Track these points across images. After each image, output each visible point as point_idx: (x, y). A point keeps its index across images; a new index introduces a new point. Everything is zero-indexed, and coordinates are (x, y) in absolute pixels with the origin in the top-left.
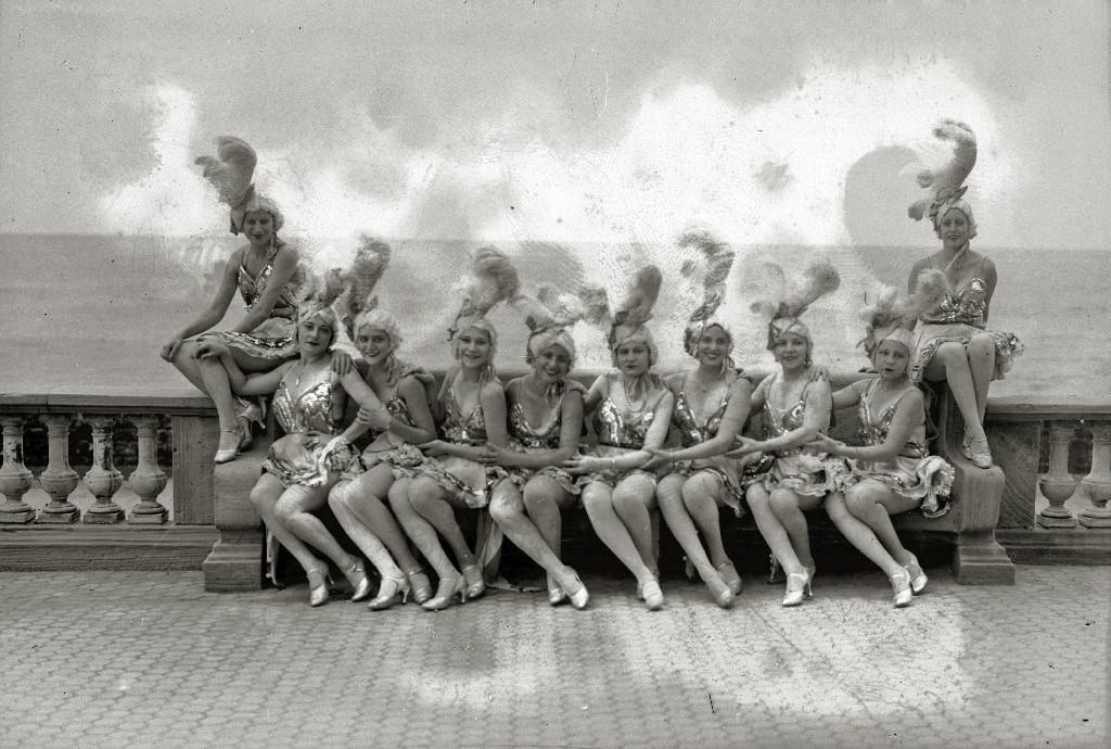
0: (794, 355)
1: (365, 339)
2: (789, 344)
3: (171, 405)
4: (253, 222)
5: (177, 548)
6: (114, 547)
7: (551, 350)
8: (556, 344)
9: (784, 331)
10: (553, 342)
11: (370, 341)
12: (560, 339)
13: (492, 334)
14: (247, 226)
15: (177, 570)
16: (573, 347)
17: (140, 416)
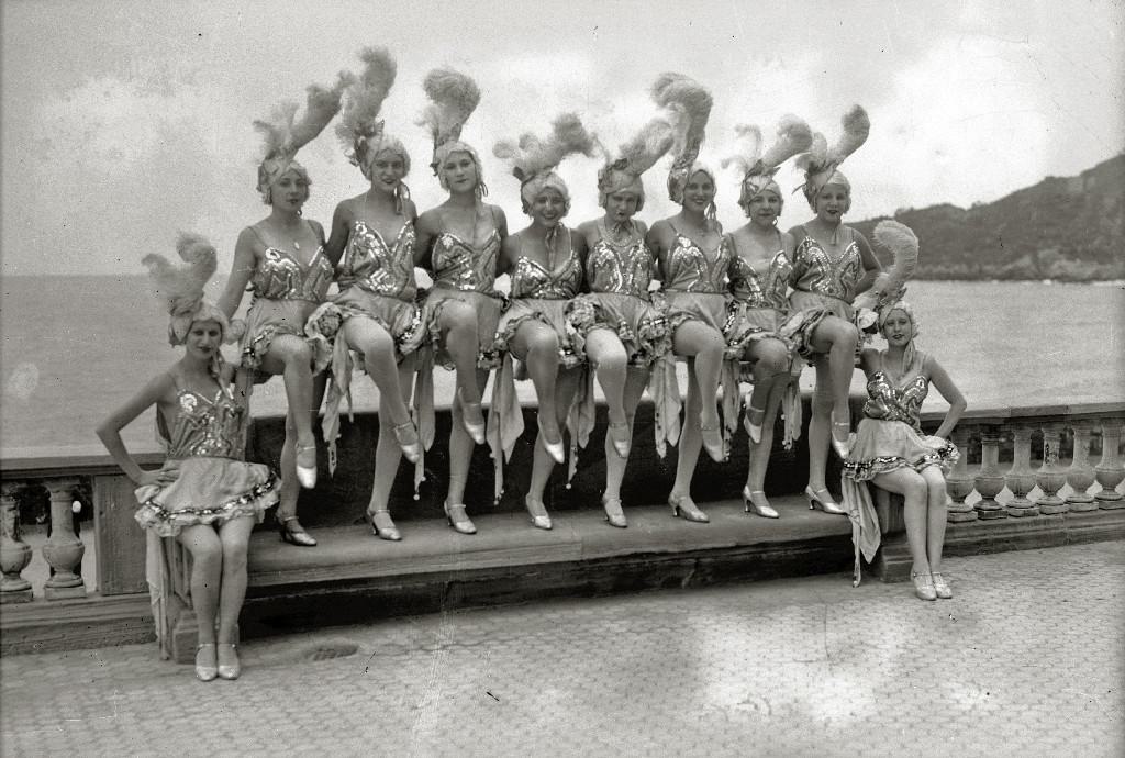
0: (770, 212)
1: (383, 164)
2: (766, 201)
3: (99, 464)
4: (200, 333)
5: (110, 622)
6: (36, 627)
7: (545, 194)
8: (548, 187)
9: (761, 188)
10: (544, 185)
11: (390, 167)
12: (550, 183)
13: (473, 152)
14: (193, 338)
15: (111, 645)
16: (563, 186)
17: (57, 479)
